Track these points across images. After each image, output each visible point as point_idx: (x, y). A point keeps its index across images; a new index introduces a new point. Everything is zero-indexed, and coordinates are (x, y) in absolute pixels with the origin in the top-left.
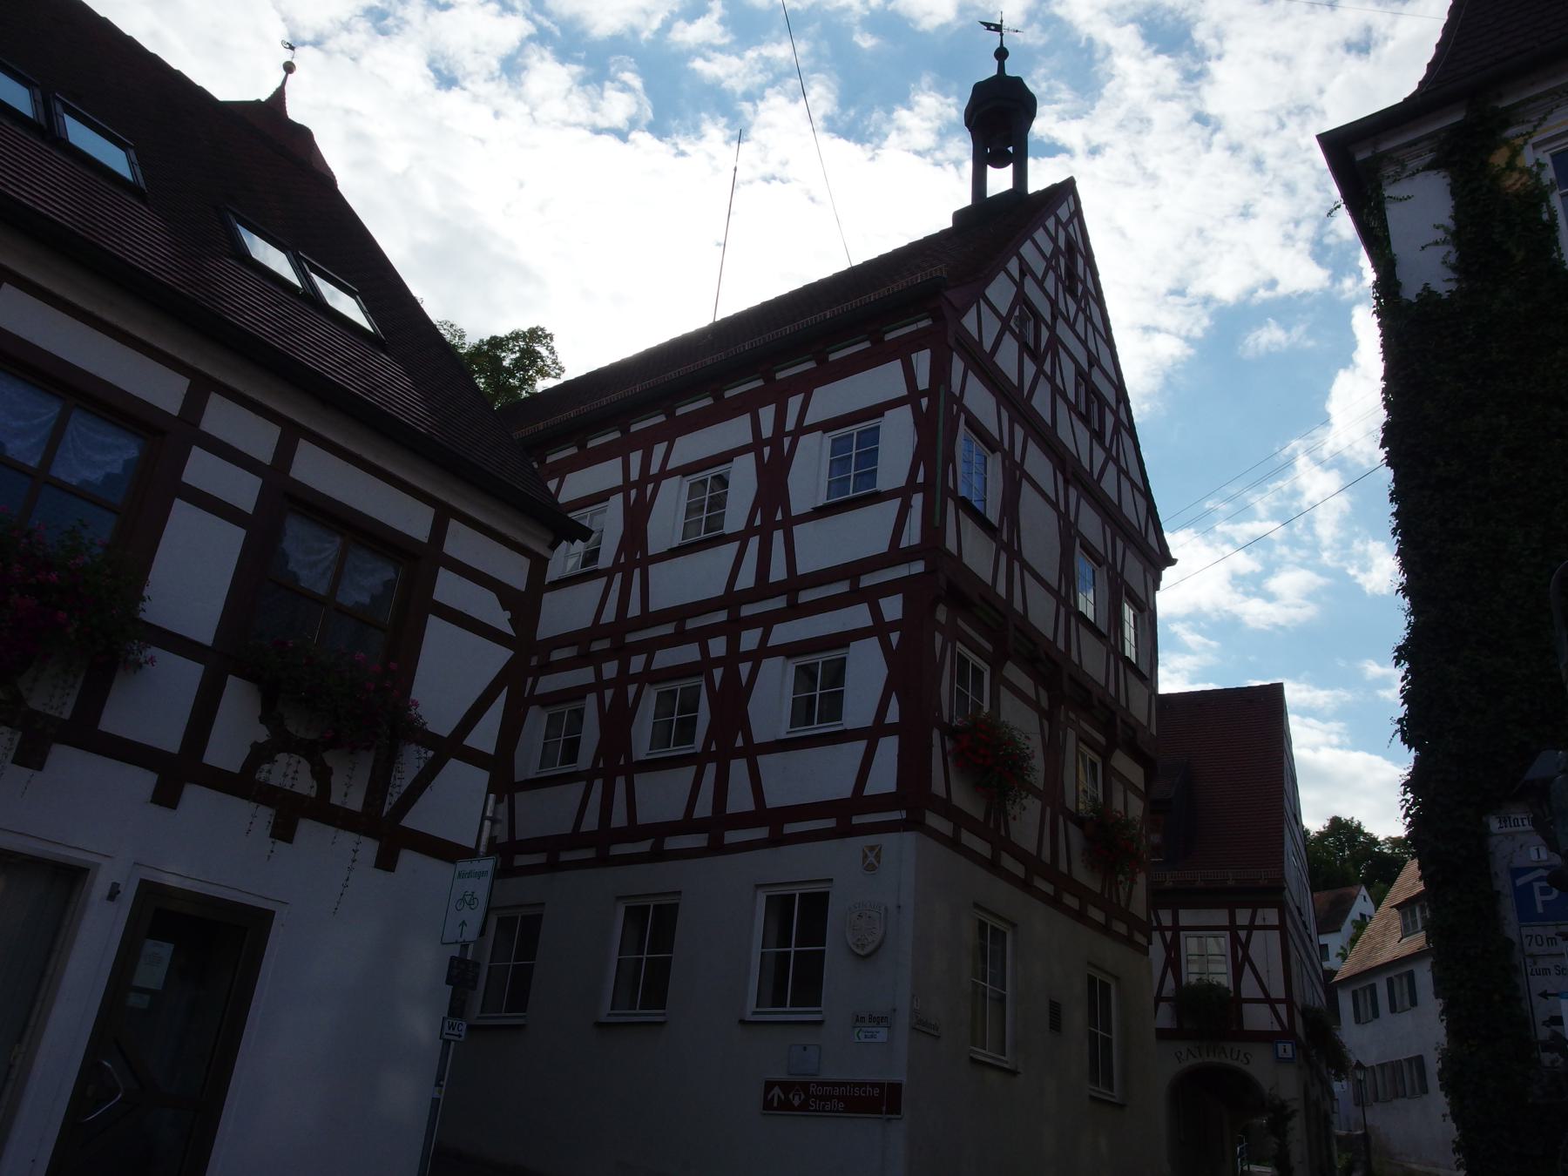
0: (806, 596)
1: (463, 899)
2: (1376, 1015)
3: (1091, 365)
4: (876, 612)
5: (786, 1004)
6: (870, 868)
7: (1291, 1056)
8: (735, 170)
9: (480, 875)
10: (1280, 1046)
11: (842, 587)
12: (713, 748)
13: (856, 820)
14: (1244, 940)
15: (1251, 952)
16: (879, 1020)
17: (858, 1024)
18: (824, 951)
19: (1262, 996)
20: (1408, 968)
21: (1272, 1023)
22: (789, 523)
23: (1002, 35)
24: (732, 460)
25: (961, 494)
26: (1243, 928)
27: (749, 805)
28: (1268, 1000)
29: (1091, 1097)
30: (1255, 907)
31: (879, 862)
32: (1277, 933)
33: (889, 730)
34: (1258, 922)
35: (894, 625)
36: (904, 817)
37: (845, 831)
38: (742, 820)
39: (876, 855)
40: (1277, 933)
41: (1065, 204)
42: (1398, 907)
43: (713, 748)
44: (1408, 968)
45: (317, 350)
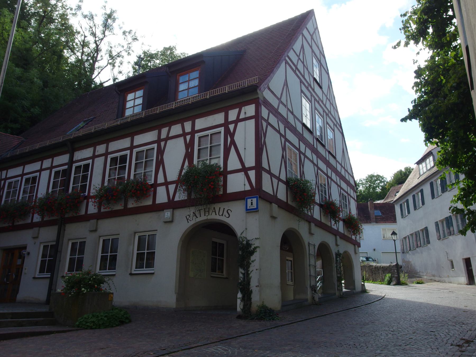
7: (255, 207)
10: (249, 201)
20: (421, 188)
28: (245, 170)
30: (240, 106)
41: (311, 21)
44: (421, 188)
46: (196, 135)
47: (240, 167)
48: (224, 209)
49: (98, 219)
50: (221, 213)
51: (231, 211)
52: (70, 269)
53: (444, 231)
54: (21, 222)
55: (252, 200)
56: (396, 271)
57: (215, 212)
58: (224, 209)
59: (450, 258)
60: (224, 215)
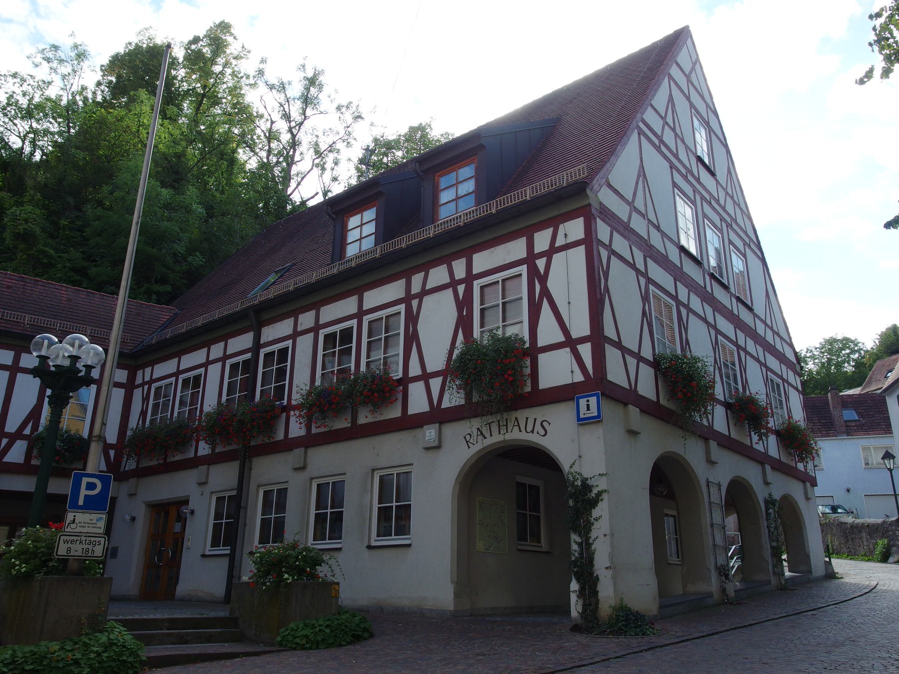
5: (520, 541)
7: (596, 414)
10: (583, 402)
14: (542, 271)
28: (571, 343)
46: (475, 283)
49: (307, 447)
50: (529, 429)
52: (263, 540)
54: (179, 457)
57: (519, 425)
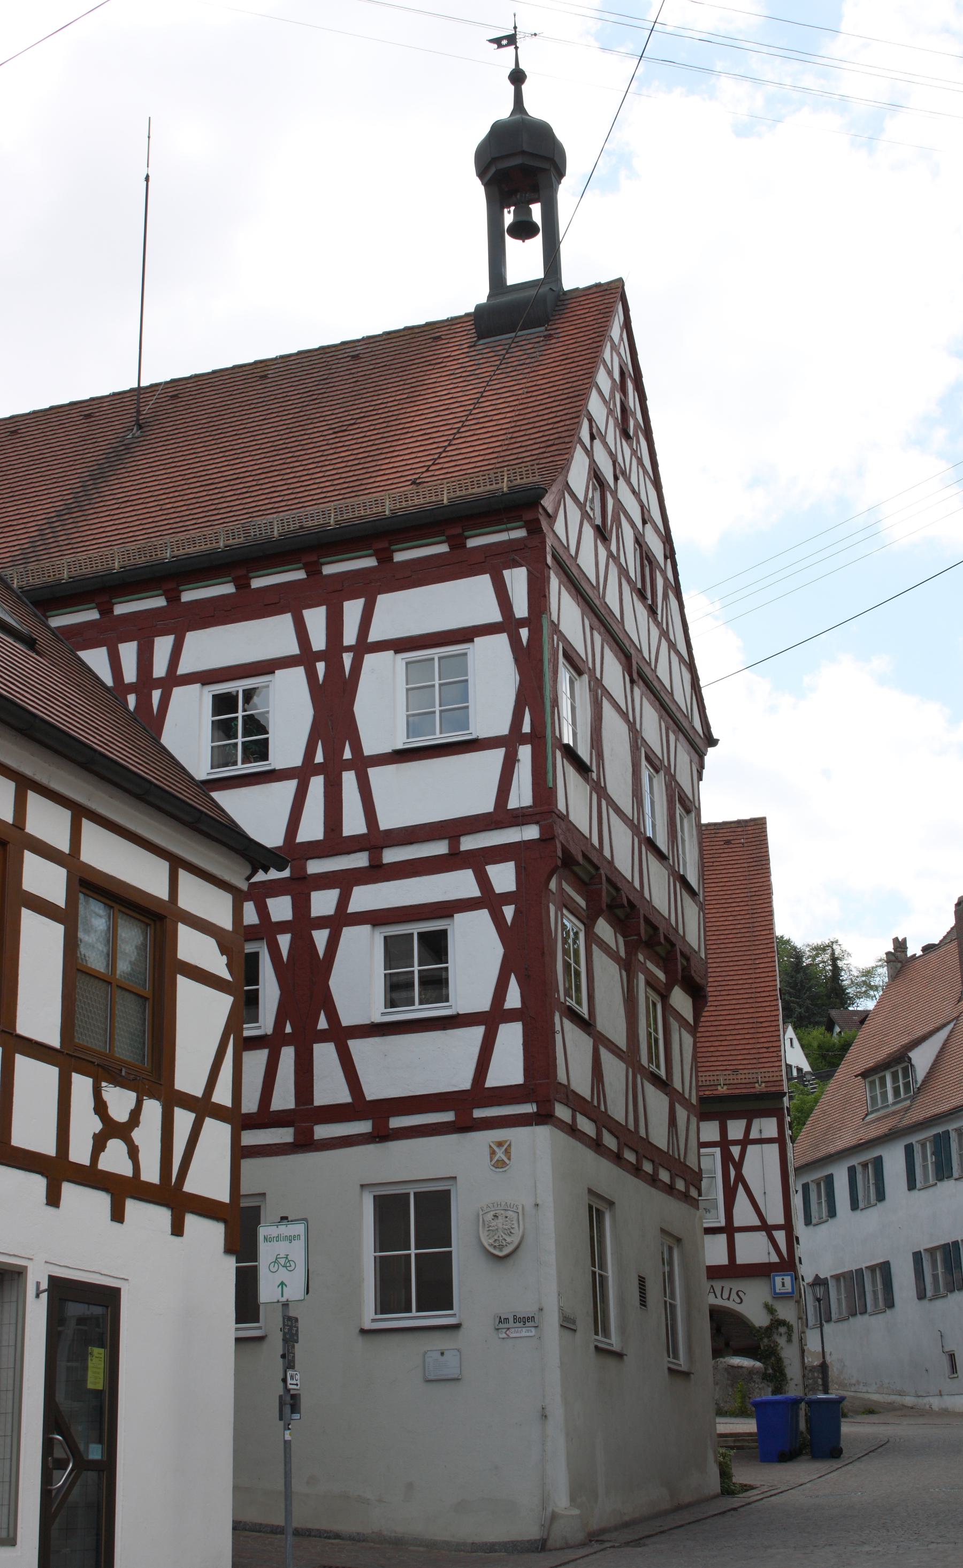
0: (391, 856)
1: (276, 1261)
2: (832, 1213)
3: (644, 522)
4: (483, 881)
6: (500, 1164)
7: (790, 1290)
8: (147, 178)
9: (291, 1239)
10: (778, 1280)
11: (440, 848)
12: (288, 1029)
13: (478, 1113)
14: (737, 1158)
15: (745, 1171)
16: (525, 1321)
17: (501, 1326)
18: (450, 1252)
19: (758, 1223)
20: (875, 1154)
21: (769, 1253)
22: (362, 764)
23: (516, 48)
24: (274, 672)
25: (565, 741)
26: (735, 1143)
27: (343, 1096)
28: (765, 1227)
29: (669, 1369)
30: (750, 1116)
31: (509, 1159)
32: (775, 1148)
33: (511, 1016)
34: (754, 1135)
35: (507, 898)
36: (535, 1110)
37: (464, 1125)
38: (335, 1113)
39: (506, 1150)
40: (775, 1148)
42: (864, 1075)
43: (288, 1029)
44: (875, 1154)
45: (148, 759)
47: (354, 1045)
48: (731, 1289)
51: (745, 1294)
53: (935, 1277)
55: (783, 1279)
56: (820, 1381)
58: (731, 1289)
59: (946, 1349)
60: (731, 1299)
